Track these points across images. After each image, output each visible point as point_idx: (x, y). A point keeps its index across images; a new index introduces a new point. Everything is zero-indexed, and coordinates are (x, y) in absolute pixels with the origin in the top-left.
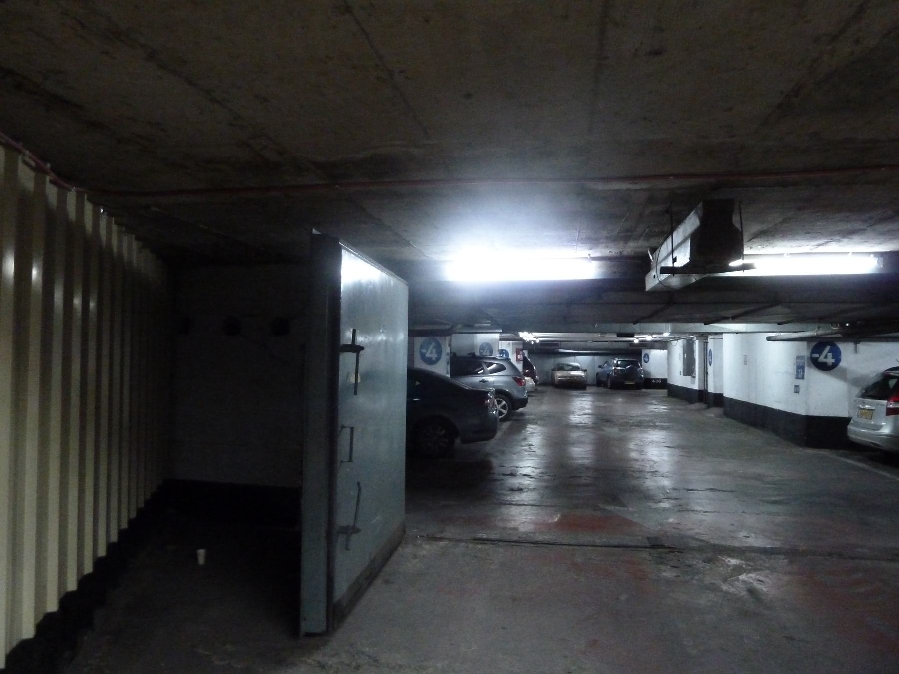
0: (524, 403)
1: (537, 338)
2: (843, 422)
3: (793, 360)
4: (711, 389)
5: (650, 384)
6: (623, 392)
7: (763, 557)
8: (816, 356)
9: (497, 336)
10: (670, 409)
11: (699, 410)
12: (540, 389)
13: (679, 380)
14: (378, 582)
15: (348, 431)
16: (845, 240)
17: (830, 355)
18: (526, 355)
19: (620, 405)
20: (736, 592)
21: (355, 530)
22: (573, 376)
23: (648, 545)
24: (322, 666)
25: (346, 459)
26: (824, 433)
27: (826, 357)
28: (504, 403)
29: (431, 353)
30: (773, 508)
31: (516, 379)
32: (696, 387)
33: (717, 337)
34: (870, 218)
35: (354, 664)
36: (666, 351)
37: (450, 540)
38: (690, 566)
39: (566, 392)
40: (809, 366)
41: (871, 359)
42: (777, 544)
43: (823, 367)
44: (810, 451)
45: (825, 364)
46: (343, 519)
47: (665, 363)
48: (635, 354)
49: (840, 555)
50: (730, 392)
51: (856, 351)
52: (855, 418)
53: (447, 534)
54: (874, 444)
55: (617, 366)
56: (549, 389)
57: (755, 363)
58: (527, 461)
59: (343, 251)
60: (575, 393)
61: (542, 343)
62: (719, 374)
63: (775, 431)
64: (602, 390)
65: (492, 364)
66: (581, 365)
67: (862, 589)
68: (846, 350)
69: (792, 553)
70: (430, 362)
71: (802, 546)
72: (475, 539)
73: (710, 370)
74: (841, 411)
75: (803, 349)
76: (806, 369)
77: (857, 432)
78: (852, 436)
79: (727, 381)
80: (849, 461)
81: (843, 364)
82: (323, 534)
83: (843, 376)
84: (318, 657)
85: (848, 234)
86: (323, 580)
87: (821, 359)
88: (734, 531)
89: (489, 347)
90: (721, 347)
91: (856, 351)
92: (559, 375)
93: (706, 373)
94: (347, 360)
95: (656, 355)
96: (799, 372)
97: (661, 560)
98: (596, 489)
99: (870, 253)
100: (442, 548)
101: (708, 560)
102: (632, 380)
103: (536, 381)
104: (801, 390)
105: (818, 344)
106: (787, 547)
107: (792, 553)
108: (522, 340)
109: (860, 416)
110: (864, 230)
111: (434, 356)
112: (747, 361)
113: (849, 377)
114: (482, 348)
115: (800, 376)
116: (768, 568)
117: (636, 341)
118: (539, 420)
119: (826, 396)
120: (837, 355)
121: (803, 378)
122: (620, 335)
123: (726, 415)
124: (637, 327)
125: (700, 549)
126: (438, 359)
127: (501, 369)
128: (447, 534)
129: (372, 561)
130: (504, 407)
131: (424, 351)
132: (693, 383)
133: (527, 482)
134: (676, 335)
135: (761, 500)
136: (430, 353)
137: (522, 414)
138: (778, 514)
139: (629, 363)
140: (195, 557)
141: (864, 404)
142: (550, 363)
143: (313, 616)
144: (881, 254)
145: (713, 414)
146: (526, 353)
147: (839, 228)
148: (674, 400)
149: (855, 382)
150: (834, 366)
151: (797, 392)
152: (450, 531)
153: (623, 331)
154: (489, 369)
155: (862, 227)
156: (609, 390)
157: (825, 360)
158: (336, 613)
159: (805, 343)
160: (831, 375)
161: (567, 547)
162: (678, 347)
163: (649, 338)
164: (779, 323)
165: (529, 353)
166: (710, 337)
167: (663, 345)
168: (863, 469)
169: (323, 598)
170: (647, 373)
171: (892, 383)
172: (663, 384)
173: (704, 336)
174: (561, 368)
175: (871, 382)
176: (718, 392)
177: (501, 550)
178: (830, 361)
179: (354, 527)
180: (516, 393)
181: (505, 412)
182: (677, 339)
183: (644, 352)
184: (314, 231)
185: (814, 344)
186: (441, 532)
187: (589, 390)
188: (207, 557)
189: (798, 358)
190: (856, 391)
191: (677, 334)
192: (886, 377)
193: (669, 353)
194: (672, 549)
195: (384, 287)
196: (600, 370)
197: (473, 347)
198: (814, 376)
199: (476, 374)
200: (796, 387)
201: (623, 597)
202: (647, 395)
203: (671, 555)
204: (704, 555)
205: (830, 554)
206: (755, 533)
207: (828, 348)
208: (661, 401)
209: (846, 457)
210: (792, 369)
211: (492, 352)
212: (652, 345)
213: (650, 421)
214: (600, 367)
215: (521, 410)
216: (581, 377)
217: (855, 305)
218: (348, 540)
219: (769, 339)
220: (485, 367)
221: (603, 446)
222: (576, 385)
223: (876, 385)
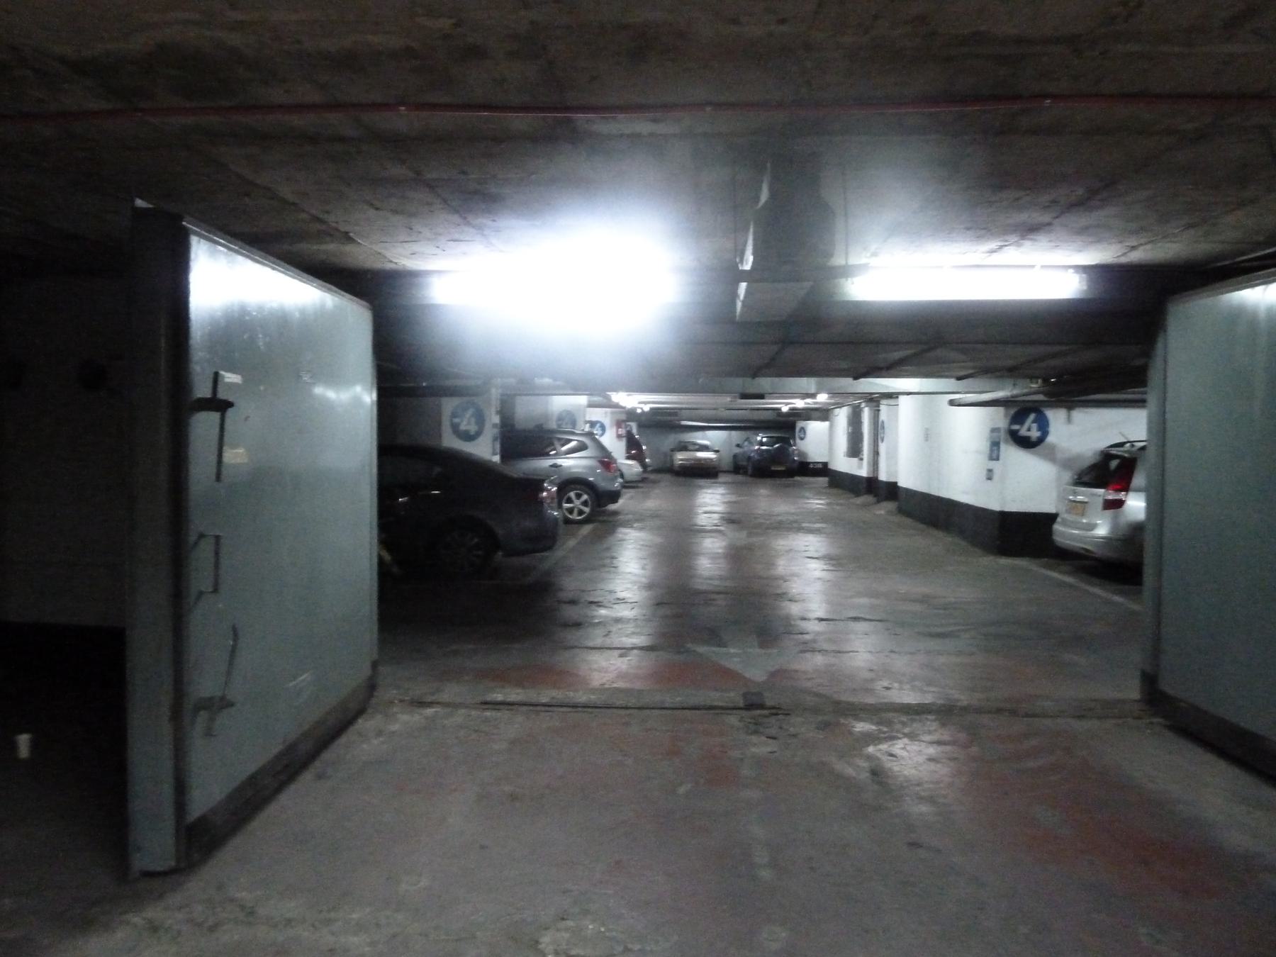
0: (614, 496)
1: (645, 403)
2: (1049, 519)
3: (986, 432)
4: (883, 477)
5: (807, 469)
6: (769, 481)
7: (904, 719)
8: (1016, 427)
9: (583, 400)
10: (828, 504)
11: (864, 506)
12: (652, 477)
13: (843, 464)
14: (307, 777)
15: (212, 541)
16: (1027, 243)
17: (1035, 426)
18: (634, 431)
19: (767, 501)
20: (854, 774)
21: (224, 703)
22: (700, 460)
23: (741, 705)
24: (154, 928)
25: (206, 585)
26: (1022, 535)
27: (1029, 430)
28: (585, 497)
29: (469, 423)
30: (933, 644)
31: (602, 463)
32: (864, 472)
33: (891, 402)
34: (1054, 202)
35: (210, 922)
36: (827, 424)
37: (447, 705)
38: (795, 736)
39: (689, 480)
40: (1006, 442)
41: (1087, 430)
42: (928, 699)
43: (1025, 443)
44: (1004, 561)
45: (1029, 438)
46: (204, 685)
47: (823, 441)
48: (786, 426)
49: (1013, 713)
50: (908, 479)
51: (1069, 420)
52: (1064, 516)
53: (445, 697)
54: (1087, 550)
55: (762, 444)
56: (667, 477)
57: (938, 437)
58: (626, 576)
59: (194, 240)
60: (701, 482)
61: (655, 412)
62: (893, 456)
63: (961, 533)
64: (740, 478)
65: (570, 441)
66: (712, 443)
67: (1031, 764)
68: (1056, 417)
69: (945, 712)
70: (469, 437)
71: (964, 699)
72: (486, 703)
73: (883, 448)
74: (1045, 505)
75: (998, 417)
76: (1003, 446)
77: (1065, 533)
78: (1058, 539)
79: (904, 466)
80: (1055, 575)
81: (1051, 439)
82: (165, 711)
83: (1051, 456)
84: (153, 912)
85: (1029, 231)
86: (167, 789)
87: (1023, 432)
88: (872, 680)
89: (569, 418)
90: (895, 417)
91: (1069, 420)
92: (680, 457)
93: (876, 453)
94: (203, 425)
95: (815, 429)
96: (994, 452)
97: (756, 728)
98: (713, 618)
99: (1070, 267)
100: (427, 718)
101: (825, 726)
102: (780, 464)
103: (644, 465)
104: (996, 477)
105: (1020, 411)
106: (940, 702)
107: (945, 712)
108: (617, 406)
109: (1068, 511)
110: (1049, 224)
111: (473, 428)
112: (930, 435)
113: (1059, 456)
114: (560, 419)
115: (994, 456)
116: (906, 735)
117: (785, 409)
118: (637, 521)
119: (1028, 484)
120: (1044, 426)
121: (998, 459)
122: (745, 396)
123: (901, 511)
124: (765, 383)
125: (816, 711)
126: (478, 434)
127: (582, 447)
128: (445, 697)
129: (290, 749)
130: (585, 503)
131: (456, 420)
132: (860, 467)
133: (625, 612)
134: (837, 400)
135: (919, 633)
136: (467, 424)
137: (615, 513)
138: (939, 653)
139: (778, 440)
140: (13, 746)
141: (1075, 494)
142: (671, 439)
143: (154, 843)
144: (1085, 269)
145: (884, 510)
146: (634, 427)
147: (1011, 221)
148: (835, 491)
149: (1066, 464)
150: (1041, 440)
151: (989, 478)
152: (451, 692)
153: (751, 391)
154: (564, 448)
155: (1046, 218)
156: (749, 479)
157: (1028, 434)
158: (201, 840)
159: (1001, 410)
160: (1033, 454)
161: (623, 712)
162: (842, 416)
163: (799, 404)
164: (959, 379)
165: (640, 426)
166: (884, 402)
167: (823, 414)
168: (1071, 586)
169: (169, 811)
170: (802, 454)
171: (1114, 464)
172: (823, 470)
173: (874, 400)
174: (684, 447)
175: (1087, 463)
176: (892, 480)
177: (520, 719)
178: (1035, 434)
179: (223, 698)
180: (603, 485)
181: (587, 510)
182: (840, 406)
183: (800, 424)
184: (140, 203)
185: (1012, 411)
186: (433, 694)
187: (722, 478)
188: (34, 745)
189: (994, 430)
190: (1068, 476)
191: (840, 397)
192: (1106, 456)
193: (831, 427)
194: (776, 711)
195: (321, 313)
196: (737, 450)
197: (546, 416)
198: (1013, 455)
199: (547, 454)
200: (990, 471)
201: (682, 790)
202: (800, 485)
203: (773, 720)
204: (820, 718)
205: (999, 711)
206: (901, 682)
207: (1032, 416)
208: (819, 494)
209: (1050, 567)
210: (984, 445)
211: (574, 424)
212: (808, 414)
213: (796, 522)
214: (738, 446)
215: (612, 507)
216: (711, 460)
217: (1064, 348)
218: (212, 719)
219: (952, 403)
220: (557, 444)
221: (737, 556)
222: (705, 472)
223: (1094, 467)
